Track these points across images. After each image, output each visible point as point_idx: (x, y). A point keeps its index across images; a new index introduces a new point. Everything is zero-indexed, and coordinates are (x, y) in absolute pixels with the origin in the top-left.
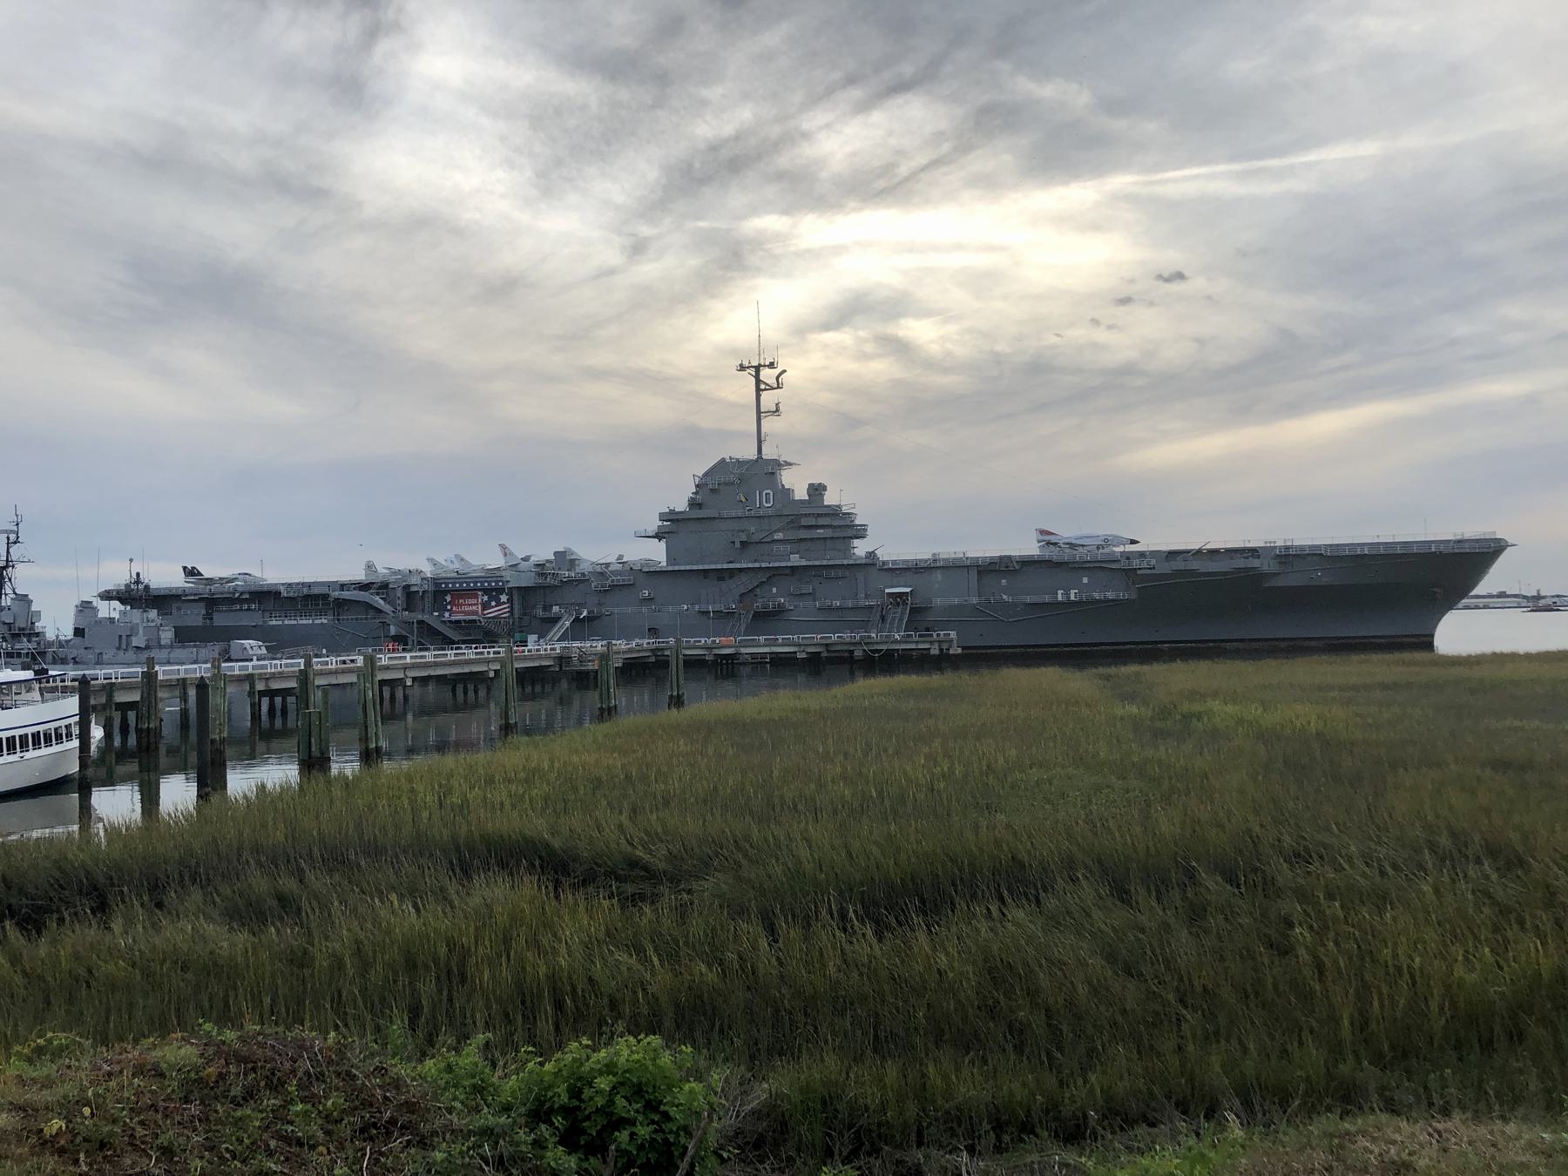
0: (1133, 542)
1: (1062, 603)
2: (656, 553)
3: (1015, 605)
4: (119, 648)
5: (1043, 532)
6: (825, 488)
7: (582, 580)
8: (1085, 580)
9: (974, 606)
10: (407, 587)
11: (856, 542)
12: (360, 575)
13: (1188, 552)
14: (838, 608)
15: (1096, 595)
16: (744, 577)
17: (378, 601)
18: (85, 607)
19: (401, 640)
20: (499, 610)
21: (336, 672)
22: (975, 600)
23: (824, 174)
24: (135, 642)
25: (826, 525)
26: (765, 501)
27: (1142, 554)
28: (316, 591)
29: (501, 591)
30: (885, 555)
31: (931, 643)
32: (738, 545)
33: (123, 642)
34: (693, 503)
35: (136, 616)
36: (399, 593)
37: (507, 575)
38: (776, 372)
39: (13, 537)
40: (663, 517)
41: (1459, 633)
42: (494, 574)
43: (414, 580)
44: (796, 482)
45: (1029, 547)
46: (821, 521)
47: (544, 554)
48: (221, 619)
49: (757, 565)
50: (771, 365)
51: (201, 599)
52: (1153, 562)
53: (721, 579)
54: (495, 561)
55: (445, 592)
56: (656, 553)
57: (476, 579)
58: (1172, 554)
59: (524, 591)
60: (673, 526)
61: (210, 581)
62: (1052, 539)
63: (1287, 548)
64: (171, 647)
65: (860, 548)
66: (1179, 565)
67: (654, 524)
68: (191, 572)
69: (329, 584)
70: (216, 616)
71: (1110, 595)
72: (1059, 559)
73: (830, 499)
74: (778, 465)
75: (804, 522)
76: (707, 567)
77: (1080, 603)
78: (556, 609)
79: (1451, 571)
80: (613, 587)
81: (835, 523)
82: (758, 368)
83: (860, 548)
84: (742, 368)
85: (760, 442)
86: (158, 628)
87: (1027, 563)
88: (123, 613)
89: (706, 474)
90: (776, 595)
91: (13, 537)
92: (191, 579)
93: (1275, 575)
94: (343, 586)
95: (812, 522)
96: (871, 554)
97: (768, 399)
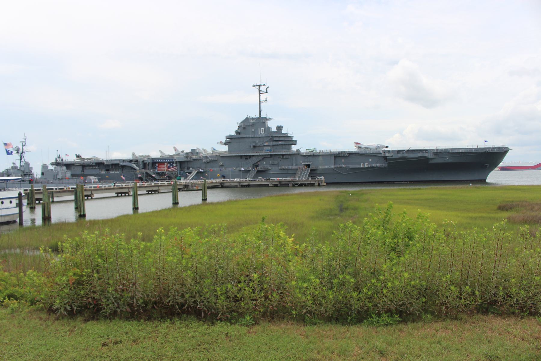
0: (387, 147)
1: (362, 168)
2: (225, 148)
3: (346, 169)
5: (357, 143)
6: (282, 127)
7: (200, 159)
8: (370, 160)
10: (143, 161)
11: (293, 146)
12: (130, 157)
13: (404, 150)
14: (286, 169)
15: (374, 165)
16: (254, 158)
17: (134, 166)
18: (45, 166)
19: (141, 179)
20: (173, 169)
21: (154, 186)
22: (333, 167)
24: (58, 177)
25: (282, 140)
26: (261, 131)
27: (389, 151)
28: (115, 162)
29: (173, 162)
30: (303, 151)
31: (315, 181)
32: (252, 147)
33: (55, 177)
34: (237, 133)
35: (59, 168)
36: (141, 163)
37: (175, 157)
38: (266, 87)
39: (24, 143)
40: (227, 137)
41: (494, 177)
42: (171, 157)
43: (146, 159)
44: (272, 125)
45: (353, 148)
46: (281, 139)
47: (188, 150)
48: (86, 172)
49: (258, 154)
50: (264, 85)
51: (81, 165)
52: (392, 154)
53: (246, 159)
54: (172, 152)
55: (156, 163)
56: (225, 148)
57: (165, 159)
58: (399, 151)
59: (181, 163)
60: (230, 140)
61: (84, 159)
62: (360, 145)
63: (437, 150)
65: (295, 148)
66: (400, 155)
67: (224, 140)
68: (78, 156)
69: (119, 160)
70: (85, 170)
71: (378, 165)
72: (362, 153)
73: (284, 131)
74: (266, 119)
75: (275, 139)
76: (241, 155)
77: (368, 168)
78: (191, 169)
79: (485, 160)
80: (210, 161)
81: (286, 139)
82: (259, 86)
83: (295, 148)
84: (254, 86)
85: (260, 111)
86: (66, 172)
87: (350, 154)
88: (55, 168)
89: (242, 123)
91: (24, 143)
92: (78, 158)
93: (432, 159)
94: (124, 161)
95: (278, 139)
96: (298, 151)
97: (263, 97)
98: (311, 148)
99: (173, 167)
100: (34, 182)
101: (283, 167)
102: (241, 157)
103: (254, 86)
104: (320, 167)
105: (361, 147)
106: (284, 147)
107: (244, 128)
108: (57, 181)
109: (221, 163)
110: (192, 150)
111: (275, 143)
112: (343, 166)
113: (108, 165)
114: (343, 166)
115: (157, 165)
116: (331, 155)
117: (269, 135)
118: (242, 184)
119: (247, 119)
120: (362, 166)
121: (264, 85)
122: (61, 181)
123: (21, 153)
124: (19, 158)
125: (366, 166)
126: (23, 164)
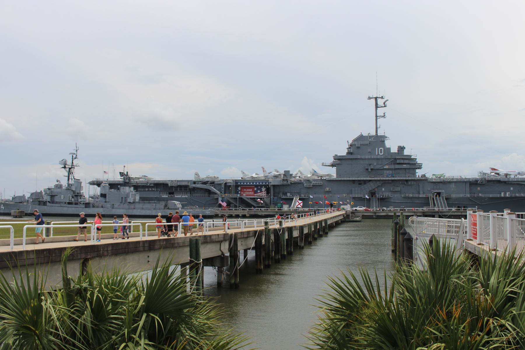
2: (333, 172)
3: (485, 198)
4: (121, 203)
8: (512, 189)
9: (468, 198)
11: (417, 171)
14: (412, 198)
15: (517, 195)
17: (213, 189)
22: (469, 196)
23: (234, 308)
26: (379, 152)
28: (183, 184)
29: (261, 186)
32: (370, 170)
34: (349, 153)
36: (223, 186)
38: (383, 100)
39: (74, 156)
44: (392, 145)
50: (382, 98)
53: (360, 184)
54: (261, 175)
56: (333, 172)
60: (339, 162)
62: (497, 172)
64: (139, 203)
65: (419, 173)
67: (331, 160)
69: (188, 181)
73: (406, 152)
75: (398, 161)
76: (354, 179)
78: (288, 194)
81: (411, 162)
82: (376, 98)
83: (419, 173)
84: (370, 98)
85: (377, 128)
90: (384, 192)
91: (74, 156)
95: (402, 161)
97: (380, 111)
98: (438, 173)
99: (261, 191)
100: (91, 205)
101: (407, 195)
102: (354, 181)
103: (370, 98)
104: (454, 196)
105: (498, 174)
106: (407, 171)
107: (358, 148)
108: (126, 206)
109: (328, 189)
110: (285, 171)
111: (397, 166)
112: (480, 195)
113: (172, 187)
114: (480, 195)
115: (239, 189)
116: (466, 182)
117: (389, 157)
118: (377, 214)
119: (361, 138)
120: (502, 195)
121: (382, 98)
122: (132, 206)
123: (70, 169)
124: (67, 174)
125: (507, 195)
126: (71, 182)
